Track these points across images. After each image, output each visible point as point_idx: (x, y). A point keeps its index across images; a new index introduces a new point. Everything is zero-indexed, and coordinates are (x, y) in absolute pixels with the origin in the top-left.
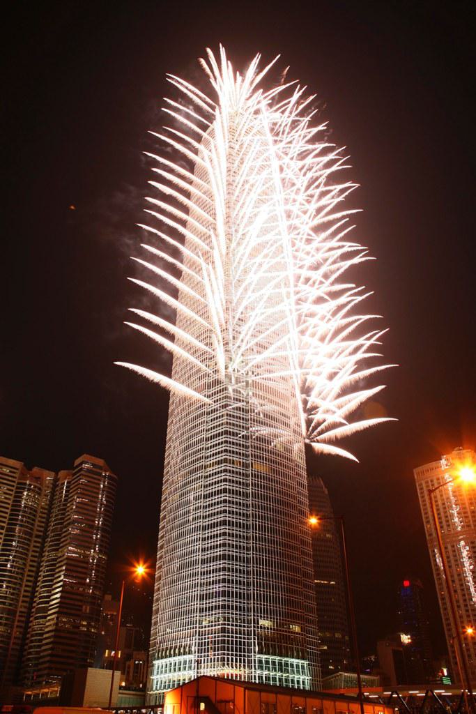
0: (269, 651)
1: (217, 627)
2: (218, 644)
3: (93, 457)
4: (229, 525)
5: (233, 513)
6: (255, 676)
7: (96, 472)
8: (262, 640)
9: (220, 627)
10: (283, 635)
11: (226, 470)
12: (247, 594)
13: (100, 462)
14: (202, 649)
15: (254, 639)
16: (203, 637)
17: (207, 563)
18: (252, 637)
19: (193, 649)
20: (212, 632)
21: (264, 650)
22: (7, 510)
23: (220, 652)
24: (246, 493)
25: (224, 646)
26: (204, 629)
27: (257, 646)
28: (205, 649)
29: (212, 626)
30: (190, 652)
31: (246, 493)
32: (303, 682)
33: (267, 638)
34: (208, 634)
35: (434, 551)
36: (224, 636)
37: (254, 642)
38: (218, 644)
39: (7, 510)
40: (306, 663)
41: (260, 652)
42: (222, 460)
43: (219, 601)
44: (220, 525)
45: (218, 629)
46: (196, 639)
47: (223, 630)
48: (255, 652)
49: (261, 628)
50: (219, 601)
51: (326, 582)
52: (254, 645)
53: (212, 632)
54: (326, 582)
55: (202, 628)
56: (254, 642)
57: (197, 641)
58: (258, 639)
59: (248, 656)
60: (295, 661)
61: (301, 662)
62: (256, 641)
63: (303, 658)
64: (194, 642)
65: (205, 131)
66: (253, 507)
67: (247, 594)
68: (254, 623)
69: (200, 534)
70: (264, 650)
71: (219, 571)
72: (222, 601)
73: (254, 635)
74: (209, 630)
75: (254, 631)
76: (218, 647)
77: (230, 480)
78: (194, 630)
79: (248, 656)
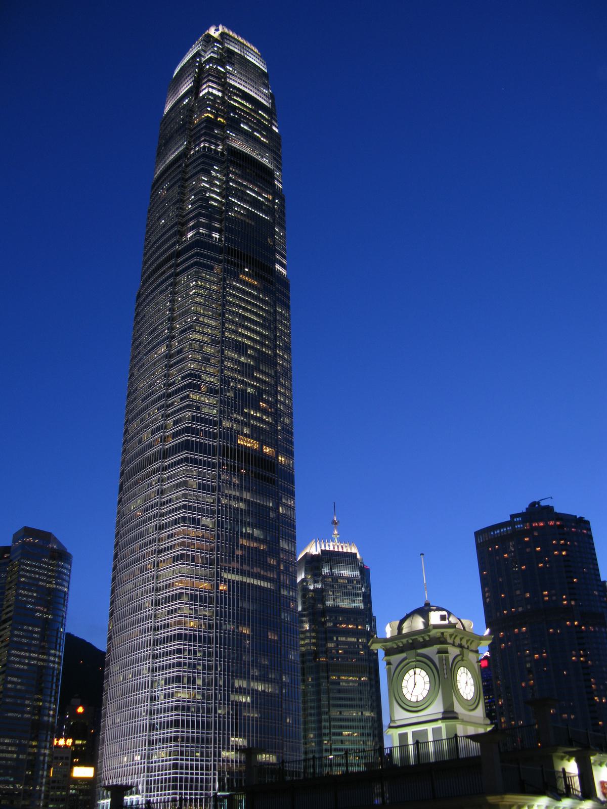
1: (168, 763)
2: (169, 782)
4: (183, 726)
5: (192, 769)
7: (186, 267)
11: (180, 663)
12: (208, 722)
14: (151, 788)
15: (214, 774)
16: (153, 774)
17: (157, 713)
18: (212, 772)
19: (140, 787)
20: (162, 768)
21: (226, 787)
25: (177, 785)
26: (153, 765)
28: (154, 787)
29: (163, 761)
30: (137, 793)
31: (209, 637)
33: (230, 772)
34: (155, 771)
35: (227, 300)
36: (176, 773)
37: (214, 779)
38: (169, 782)
42: (174, 663)
43: (171, 732)
44: (173, 682)
45: (170, 765)
46: (143, 777)
47: (175, 766)
49: (224, 761)
50: (171, 732)
53: (162, 768)
55: (152, 763)
56: (214, 779)
57: (145, 779)
62: (217, 777)
64: (142, 779)
66: (216, 656)
67: (208, 722)
68: (215, 756)
69: (149, 651)
70: (226, 787)
71: (171, 741)
72: (174, 746)
73: (215, 769)
74: (159, 766)
75: (215, 765)
76: (169, 786)
78: (143, 765)
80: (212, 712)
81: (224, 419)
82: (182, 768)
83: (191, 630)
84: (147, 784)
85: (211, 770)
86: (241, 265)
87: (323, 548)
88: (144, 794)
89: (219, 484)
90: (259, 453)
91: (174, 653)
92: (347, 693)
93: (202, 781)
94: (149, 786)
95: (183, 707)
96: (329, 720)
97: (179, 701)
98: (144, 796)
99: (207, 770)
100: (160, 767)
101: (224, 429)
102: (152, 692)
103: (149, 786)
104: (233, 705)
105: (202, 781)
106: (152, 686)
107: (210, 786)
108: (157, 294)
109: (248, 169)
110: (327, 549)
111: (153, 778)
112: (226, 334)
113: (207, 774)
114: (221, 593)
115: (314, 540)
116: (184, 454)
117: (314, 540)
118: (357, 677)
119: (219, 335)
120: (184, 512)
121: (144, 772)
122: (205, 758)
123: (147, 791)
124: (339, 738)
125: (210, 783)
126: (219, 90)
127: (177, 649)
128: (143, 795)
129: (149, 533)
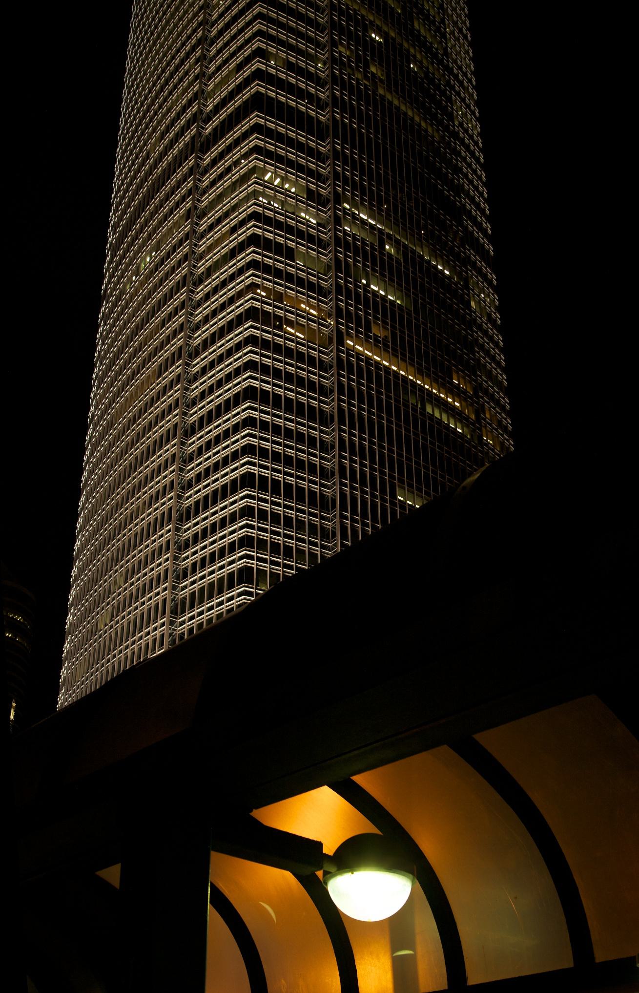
77: (263, 479)
101: (349, 355)
120: (247, 556)
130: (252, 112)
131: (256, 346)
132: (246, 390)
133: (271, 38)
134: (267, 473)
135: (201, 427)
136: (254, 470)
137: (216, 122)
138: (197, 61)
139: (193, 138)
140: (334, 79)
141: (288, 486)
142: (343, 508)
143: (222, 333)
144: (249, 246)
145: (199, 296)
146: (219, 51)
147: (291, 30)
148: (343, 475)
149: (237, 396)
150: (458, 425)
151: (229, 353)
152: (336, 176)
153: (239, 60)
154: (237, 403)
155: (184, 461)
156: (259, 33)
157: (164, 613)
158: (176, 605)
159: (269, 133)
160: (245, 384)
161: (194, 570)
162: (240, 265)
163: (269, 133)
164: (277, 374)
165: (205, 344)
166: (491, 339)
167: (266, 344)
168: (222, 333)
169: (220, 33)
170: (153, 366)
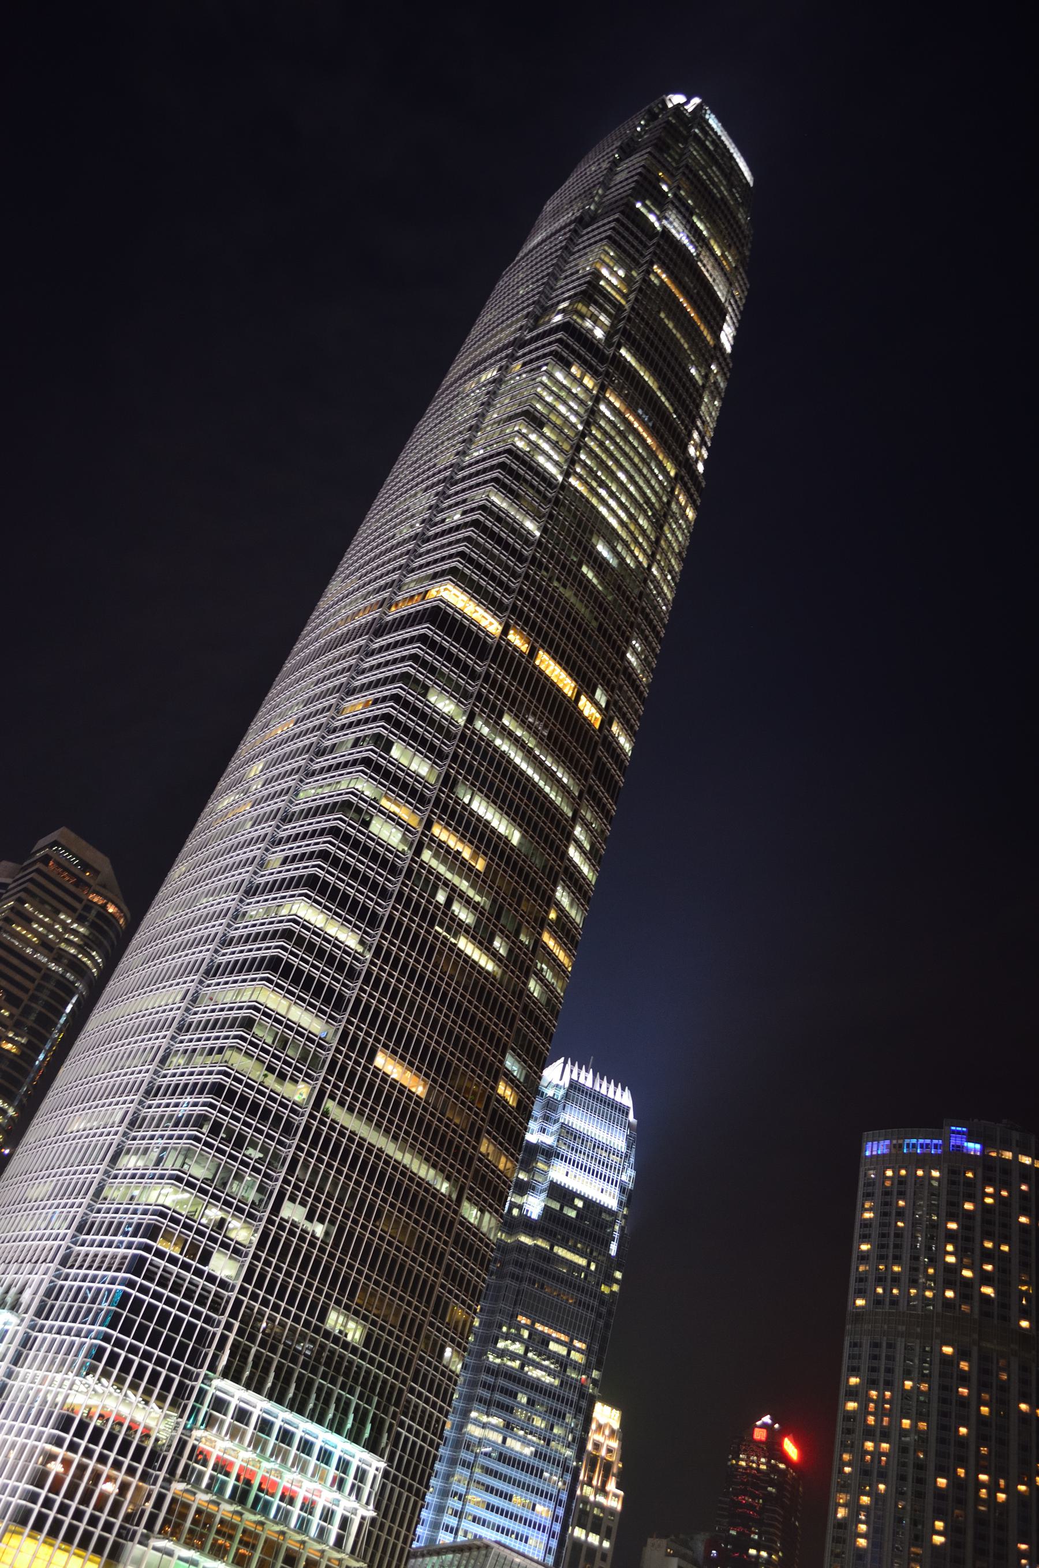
0: (261, 1383)
3: (84, 843)
6: (161, 1497)
8: (252, 1338)
9: (131, 1252)
10: (332, 1352)
13: (102, 862)
15: (228, 1327)
18: (224, 1319)
22: (27, 983)
23: (96, 1328)
24: (316, 1056)
27: (227, 1352)
31: (341, 996)
32: (345, 1523)
37: (224, 1339)
39: (27, 983)
40: (375, 1465)
41: (232, 1373)
47: (137, 1265)
48: (212, 1368)
51: (444, 1187)
52: (221, 1347)
54: (444, 1187)
56: (224, 1339)
58: (240, 1333)
59: (186, 1374)
60: (340, 1445)
61: (358, 1455)
62: (232, 1336)
63: (372, 1446)
65: (208, 1369)
73: (234, 1314)
79: (186, 1374)
80: (295, 1134)
81: (480, 714)
82: (149, 1277)
83: (251, 1088)
84: (48, 1293)
85: (223, 1314)
86: (522, 703)
87: (575, 1077)
88: (28, 1316)
89: (410, 865)
90: (417, 1103)
91: (232, 1026)
92: (513, 1466)
93: (188, 1335)
94: (50, 1302)
95: (232, 1093)
96: (458, 1514)
97: (227, 1075)
98: (51, 1272)
99: (214, 1308)
100: (107, 1260)
102: (58, 1277)
103: (50, 1302)
104: (281, 1227)
105: (188, 1335)
106: (163, 1061)
107: (206, 1355)
108: (357, 599)
109: (534, 714)
110: (582, 1080)
111: (67, 1283)
112: (427, 855)
113: (208, 1320)
114: (281, 1227)
115: (562, 1059)
116: (423, 629)
117: (562, 1059)
118: (567, 1335)
119: (462, 721)
120: (319, 866)
121: (52, 1261)
122: (183, 1364)
123: (38, 1314)
124: (507, 1400)
125: (210, 1346)
126: (557, 464)
127: (284, 930)
128: (22, 1320)
129: (163, 1003)
130: (426, 622)
131: (368, 767)
132: (421, 635)
133: (471, 560)
134: (331, 879)
135: (360, 691)
136: (321, 873)
137: (466, 473)
138: (507, 356)
139: (515, 339)
140: (629, 319)
141: (346, 896)
142: (387, 929)
143: (478, 473)
144: (409, 660)
145: (415, 565)
146: (457, 493)
147: (492, 556)
148: (398, 900)
149: (395, 676)
150: (566, 774)
151: (395, 661)
152: (455, 759)
153: (486, 465)
154: (393, 681)
155: (273, 843)
156: (462, 554)
157: (138, 1090)
158: (251, 887)
159: (432, 645)
160: (405, 670)
161: (287, 841)
162: (452, 551)
163: (432, 645)
164: (345, 868)
165: (381, 650)
166: (632, 706)
167: (406, 704)
168: (478, 473)
169: (464, 479)
170: (376, 585)
